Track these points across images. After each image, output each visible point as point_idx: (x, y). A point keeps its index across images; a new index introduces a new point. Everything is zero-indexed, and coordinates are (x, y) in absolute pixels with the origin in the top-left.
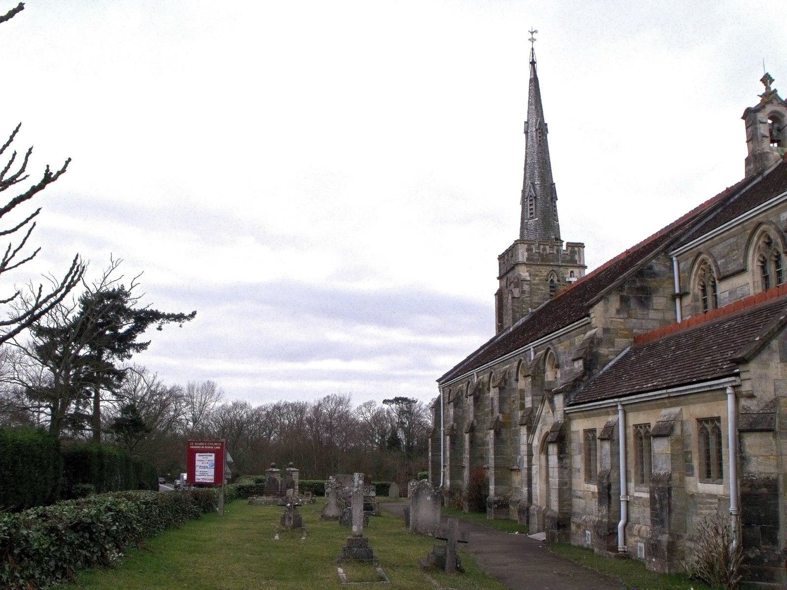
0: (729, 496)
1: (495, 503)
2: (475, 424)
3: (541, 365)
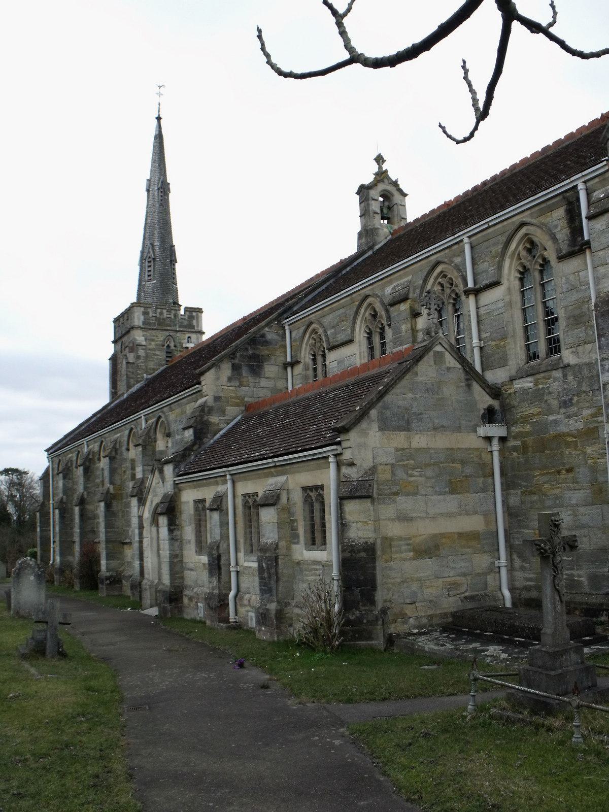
0: (332, 562)
1: (107, 578)
2: (85, 496)
3: (152, 434)
